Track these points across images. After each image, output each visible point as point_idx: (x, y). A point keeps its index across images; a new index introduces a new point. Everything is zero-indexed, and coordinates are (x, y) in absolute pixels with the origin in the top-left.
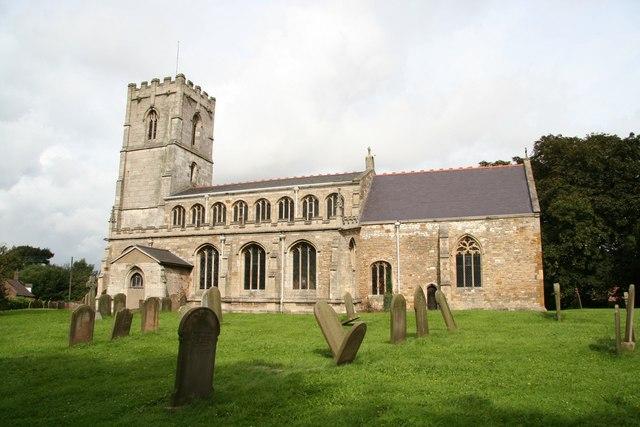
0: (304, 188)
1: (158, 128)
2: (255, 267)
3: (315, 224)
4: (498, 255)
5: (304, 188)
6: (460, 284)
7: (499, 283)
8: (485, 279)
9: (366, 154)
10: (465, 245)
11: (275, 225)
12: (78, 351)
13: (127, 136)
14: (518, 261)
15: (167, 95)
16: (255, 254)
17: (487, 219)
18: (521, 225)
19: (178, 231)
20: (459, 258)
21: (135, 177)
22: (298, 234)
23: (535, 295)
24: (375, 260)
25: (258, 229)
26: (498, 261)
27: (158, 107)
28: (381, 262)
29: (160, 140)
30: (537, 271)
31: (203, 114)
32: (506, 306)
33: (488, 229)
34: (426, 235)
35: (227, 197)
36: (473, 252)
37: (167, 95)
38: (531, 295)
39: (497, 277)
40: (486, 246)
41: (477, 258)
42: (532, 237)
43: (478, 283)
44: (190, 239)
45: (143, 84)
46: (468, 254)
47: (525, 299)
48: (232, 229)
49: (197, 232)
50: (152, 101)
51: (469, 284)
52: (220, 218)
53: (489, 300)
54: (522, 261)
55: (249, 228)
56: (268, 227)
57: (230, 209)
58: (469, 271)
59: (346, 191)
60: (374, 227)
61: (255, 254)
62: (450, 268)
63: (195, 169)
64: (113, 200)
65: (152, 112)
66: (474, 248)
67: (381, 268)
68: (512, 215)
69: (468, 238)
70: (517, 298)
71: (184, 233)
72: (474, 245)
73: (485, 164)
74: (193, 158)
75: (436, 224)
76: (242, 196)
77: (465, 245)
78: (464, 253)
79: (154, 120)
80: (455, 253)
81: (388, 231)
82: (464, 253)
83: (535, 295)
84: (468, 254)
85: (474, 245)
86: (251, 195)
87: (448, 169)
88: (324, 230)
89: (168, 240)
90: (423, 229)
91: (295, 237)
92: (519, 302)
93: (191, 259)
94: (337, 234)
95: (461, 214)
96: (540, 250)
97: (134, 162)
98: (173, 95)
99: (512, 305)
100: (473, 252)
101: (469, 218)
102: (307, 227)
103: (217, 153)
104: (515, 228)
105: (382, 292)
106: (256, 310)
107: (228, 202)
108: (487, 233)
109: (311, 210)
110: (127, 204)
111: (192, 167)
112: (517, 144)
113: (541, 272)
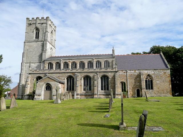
0: (96, 58)
1: (40, 35)
3: (109, 70)
5: (96, 58)
6: (147, 89)
8: (154, 87)
10: (147, 77)
11: (95, 70)
14: (164, 82)
16: (70, 79)
19: (58, 71)
20: (146, 81)
23: (169, 92)
25: (88, 71)
29: (41, 39)
30: (169, 85)
35: (69, 60)
36: (150, 79)
38: (168, 92)
41: (152, 81)
43: (152, 89)
44: (63, 74)
45: (32, 18)
48: (79, 71)
49: (65, 72)
51: (149, 89)
52: (66, 67)
53: (155, 94)
55: (85, 70)
56: (92, 70)
57: (70, 64)
61: (70, 79)
66: (150, 78)
69: (149, 75)
71: (61, 72)
72: (150, 77)
73: (128, 54)
77: (147, 77)
78: (148, 79)
79: (37, 32)
80: (145, 80)
82: (148, 79)
83: (169, 92)
85: (150, 77)
86: (78, 60)
87: (123, 55)
88: (112, 72)
91: (84, 75)
92: (164, 94)
96: (170, 79)
100: (150, 79)
102: (106, 71)
105: (105, 89)
107: (70, 62)
109: (98, 65)
113: (171, 85)
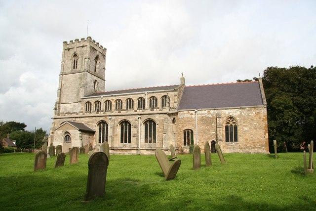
0: (150, 93)
1: (78, 63)
2: (126, 132)
3: (155, 111)
4: (246, 126)
5: (150, 93)
6: (227, 140)
7: (246, 140)
8: (239, 138)
9: (181, 76)
10: (229, 121)
11: (136, 111)
12: (39, 174)
13: (63, 67)
14: (256, 129)
15: (83, 47)
16: (126, 126)
17: (241, 108)
18: (257, 111)
19: (88, 114)
20: (227, 128)
21: (67, 87)
22: (147, 116)
23: (264, 146)
24: (185, 128)
25: (127, 113)
26: (246, 129)
27: (78, 53)
28: (188, 129)
29: (79, 69)
30: (265, 134)
31: (100, 56)
32: (250, 151)
33: (241, 113)
34: (210, 116)
35: (112, 98)
36: (233, 125)
37: (83, 47)
38: (262, 146)
39: (246, 137)
40: (240, 122)
41: (236, 128)
42: (263, 117)
43: (236, 140)
44: (94, 118)
45: (70, 41)
46: (231, 125)
47: (259, 148)
48: (115, 113)
49: (97, 115)
50: (75, 50)
51: (231, 140)
52: (108, 108)
53: (241, 148)
54: (258, 129)
55: (123, 112)
56: (132, 112)
57: (114, 103)
58: (232, 134)
59: (171, 95)
60: (185, 112)
61: (126, 126)
62: (222, 133)
63: (96, 83)
64: (56, 99)
65: (75, 55)
66: (234, 123)
67: (188, 132)
68: (253, 106)
69: (231, 117)
70: (255, 147)
71: (91, 115)
72: (234, 121)
73: (239, 81)
74: (95, 78)
75: (215, 111)
76: (120, 97)
77: (229, 121)
78: (229, 125)
79: (76, 59)
80: (224, 125)
81: (192, 114)
82: (229, 125)
83: (264, 146)
84: (231, 125)
85: (234, 121)
86: (124, 96)
87: (221, 83)
88: (160, 114)
89: (83, 119)
90: (209, 113)
91: (146, 117)
92: (256, 149)
93: (94, 128)
94: (167, 116)
95: (228, 106)
96: (267, 124)
97: (66, 80)
98: (86, 47)
99: (253, 151)
100: (233, 125)
101: (232, 108)
102: (152, 112)
103: (107, 75)
104: (254, 113)
105: (188, 144)
106: (127, 153)
107: (113, 100)
108: (240, 115)
109: (153, 104)
110: (63, 101)
111: (95, 83)
112: (255, 71)
113: (267, 134)
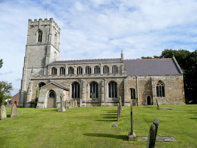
0: (104, 63)
1: (43, 38)
3: (117, 75)
5: (104, 63)
6: (158, 96)
8: (166, 94)
10: (159, 83)
11: (102, 75)
14: (176, 89)
16: (76, 86)
19: (63, 77)
20: (157, 87)
23: (182, 99)
25: (95, 77)
29: (44, 42)
30: (182, 92)
35: (74, 65)
36: (162, 86)
38: (180, 100)
41: (163, 88)
43: (164, 96)
44: (68, 80)
45: (35, 20)
48: (85, 76)
49: (71, 77)
51: (161, 96)
52: (71, 72)
53: (167, 101)
55: (92, 76)
56: (99, 76)
57: (76, 69)
61: (76, 86)
66: (162, 85)
69: (160, 81)
71: (65, 77)
72: (162, 84)
73: (138, 59)
77: (159, 83)
78: (159, 86)
79: (40, 34)
80: (156, 86)
82: (159, 86)
83: (182, 99)
85: (162, 84)
86: (84, 65)
87: (132, 59)
88: (120, 78)
91: (90, 81)
92: (177, 102)
96: (183, 85)
100: (162, 86)
102: (114, 76)
105: (113, 97)
107: (75, 67)
109: (106, 70)
113: (184, 92)
